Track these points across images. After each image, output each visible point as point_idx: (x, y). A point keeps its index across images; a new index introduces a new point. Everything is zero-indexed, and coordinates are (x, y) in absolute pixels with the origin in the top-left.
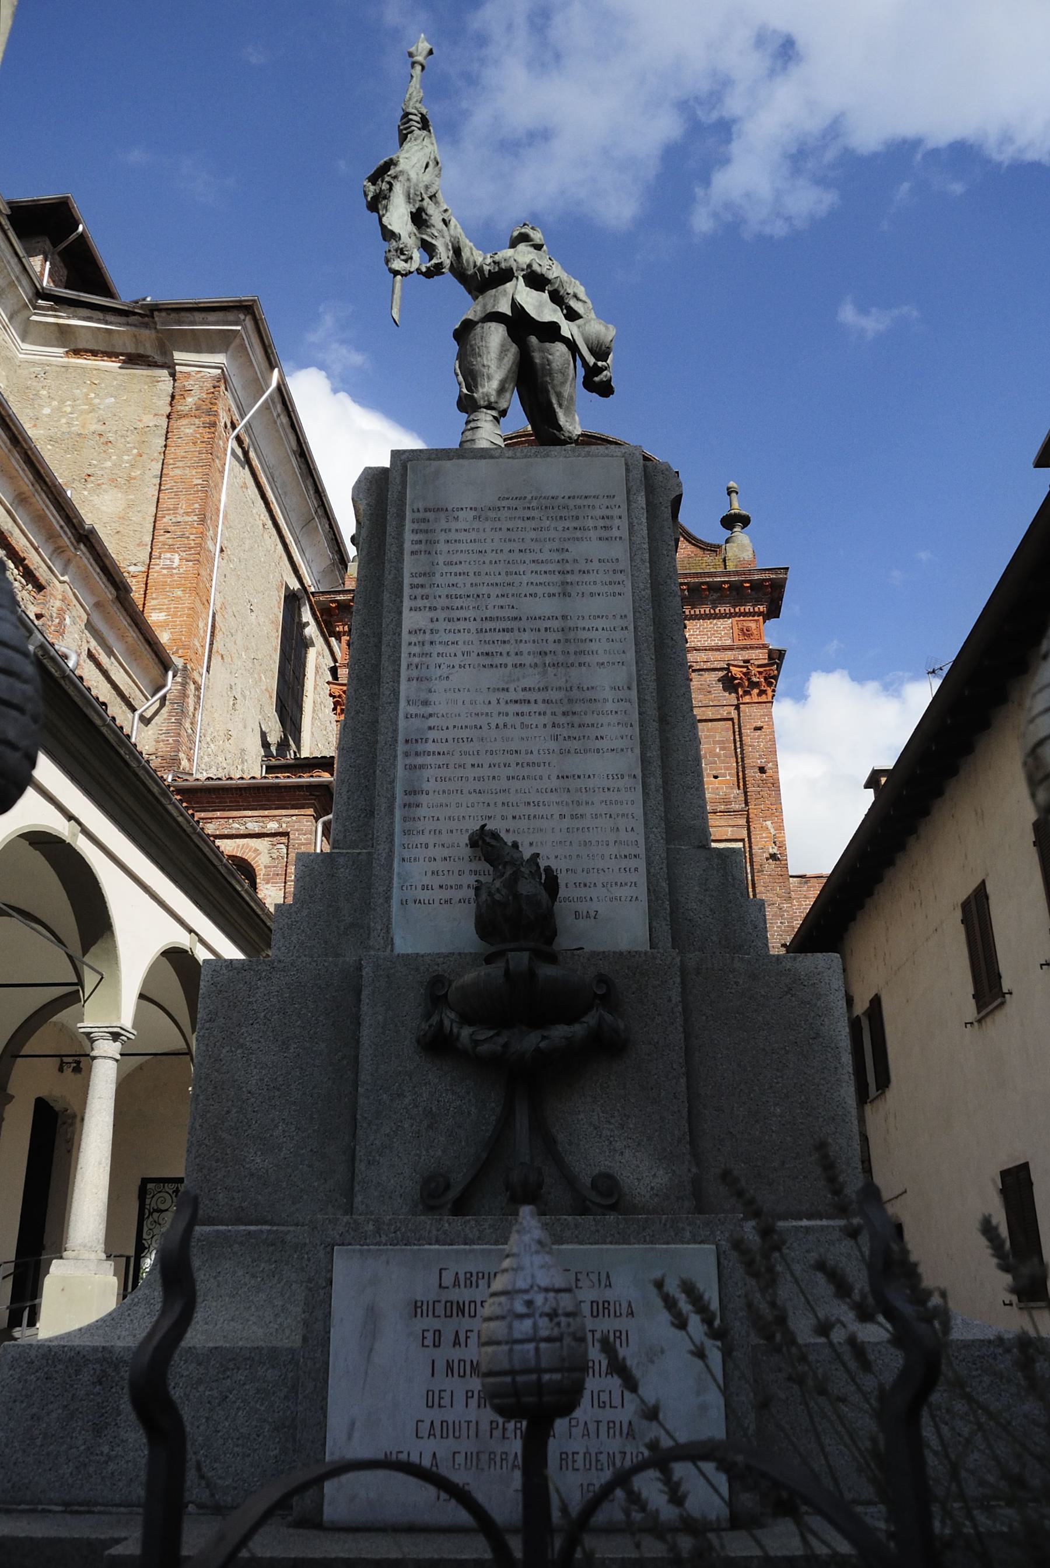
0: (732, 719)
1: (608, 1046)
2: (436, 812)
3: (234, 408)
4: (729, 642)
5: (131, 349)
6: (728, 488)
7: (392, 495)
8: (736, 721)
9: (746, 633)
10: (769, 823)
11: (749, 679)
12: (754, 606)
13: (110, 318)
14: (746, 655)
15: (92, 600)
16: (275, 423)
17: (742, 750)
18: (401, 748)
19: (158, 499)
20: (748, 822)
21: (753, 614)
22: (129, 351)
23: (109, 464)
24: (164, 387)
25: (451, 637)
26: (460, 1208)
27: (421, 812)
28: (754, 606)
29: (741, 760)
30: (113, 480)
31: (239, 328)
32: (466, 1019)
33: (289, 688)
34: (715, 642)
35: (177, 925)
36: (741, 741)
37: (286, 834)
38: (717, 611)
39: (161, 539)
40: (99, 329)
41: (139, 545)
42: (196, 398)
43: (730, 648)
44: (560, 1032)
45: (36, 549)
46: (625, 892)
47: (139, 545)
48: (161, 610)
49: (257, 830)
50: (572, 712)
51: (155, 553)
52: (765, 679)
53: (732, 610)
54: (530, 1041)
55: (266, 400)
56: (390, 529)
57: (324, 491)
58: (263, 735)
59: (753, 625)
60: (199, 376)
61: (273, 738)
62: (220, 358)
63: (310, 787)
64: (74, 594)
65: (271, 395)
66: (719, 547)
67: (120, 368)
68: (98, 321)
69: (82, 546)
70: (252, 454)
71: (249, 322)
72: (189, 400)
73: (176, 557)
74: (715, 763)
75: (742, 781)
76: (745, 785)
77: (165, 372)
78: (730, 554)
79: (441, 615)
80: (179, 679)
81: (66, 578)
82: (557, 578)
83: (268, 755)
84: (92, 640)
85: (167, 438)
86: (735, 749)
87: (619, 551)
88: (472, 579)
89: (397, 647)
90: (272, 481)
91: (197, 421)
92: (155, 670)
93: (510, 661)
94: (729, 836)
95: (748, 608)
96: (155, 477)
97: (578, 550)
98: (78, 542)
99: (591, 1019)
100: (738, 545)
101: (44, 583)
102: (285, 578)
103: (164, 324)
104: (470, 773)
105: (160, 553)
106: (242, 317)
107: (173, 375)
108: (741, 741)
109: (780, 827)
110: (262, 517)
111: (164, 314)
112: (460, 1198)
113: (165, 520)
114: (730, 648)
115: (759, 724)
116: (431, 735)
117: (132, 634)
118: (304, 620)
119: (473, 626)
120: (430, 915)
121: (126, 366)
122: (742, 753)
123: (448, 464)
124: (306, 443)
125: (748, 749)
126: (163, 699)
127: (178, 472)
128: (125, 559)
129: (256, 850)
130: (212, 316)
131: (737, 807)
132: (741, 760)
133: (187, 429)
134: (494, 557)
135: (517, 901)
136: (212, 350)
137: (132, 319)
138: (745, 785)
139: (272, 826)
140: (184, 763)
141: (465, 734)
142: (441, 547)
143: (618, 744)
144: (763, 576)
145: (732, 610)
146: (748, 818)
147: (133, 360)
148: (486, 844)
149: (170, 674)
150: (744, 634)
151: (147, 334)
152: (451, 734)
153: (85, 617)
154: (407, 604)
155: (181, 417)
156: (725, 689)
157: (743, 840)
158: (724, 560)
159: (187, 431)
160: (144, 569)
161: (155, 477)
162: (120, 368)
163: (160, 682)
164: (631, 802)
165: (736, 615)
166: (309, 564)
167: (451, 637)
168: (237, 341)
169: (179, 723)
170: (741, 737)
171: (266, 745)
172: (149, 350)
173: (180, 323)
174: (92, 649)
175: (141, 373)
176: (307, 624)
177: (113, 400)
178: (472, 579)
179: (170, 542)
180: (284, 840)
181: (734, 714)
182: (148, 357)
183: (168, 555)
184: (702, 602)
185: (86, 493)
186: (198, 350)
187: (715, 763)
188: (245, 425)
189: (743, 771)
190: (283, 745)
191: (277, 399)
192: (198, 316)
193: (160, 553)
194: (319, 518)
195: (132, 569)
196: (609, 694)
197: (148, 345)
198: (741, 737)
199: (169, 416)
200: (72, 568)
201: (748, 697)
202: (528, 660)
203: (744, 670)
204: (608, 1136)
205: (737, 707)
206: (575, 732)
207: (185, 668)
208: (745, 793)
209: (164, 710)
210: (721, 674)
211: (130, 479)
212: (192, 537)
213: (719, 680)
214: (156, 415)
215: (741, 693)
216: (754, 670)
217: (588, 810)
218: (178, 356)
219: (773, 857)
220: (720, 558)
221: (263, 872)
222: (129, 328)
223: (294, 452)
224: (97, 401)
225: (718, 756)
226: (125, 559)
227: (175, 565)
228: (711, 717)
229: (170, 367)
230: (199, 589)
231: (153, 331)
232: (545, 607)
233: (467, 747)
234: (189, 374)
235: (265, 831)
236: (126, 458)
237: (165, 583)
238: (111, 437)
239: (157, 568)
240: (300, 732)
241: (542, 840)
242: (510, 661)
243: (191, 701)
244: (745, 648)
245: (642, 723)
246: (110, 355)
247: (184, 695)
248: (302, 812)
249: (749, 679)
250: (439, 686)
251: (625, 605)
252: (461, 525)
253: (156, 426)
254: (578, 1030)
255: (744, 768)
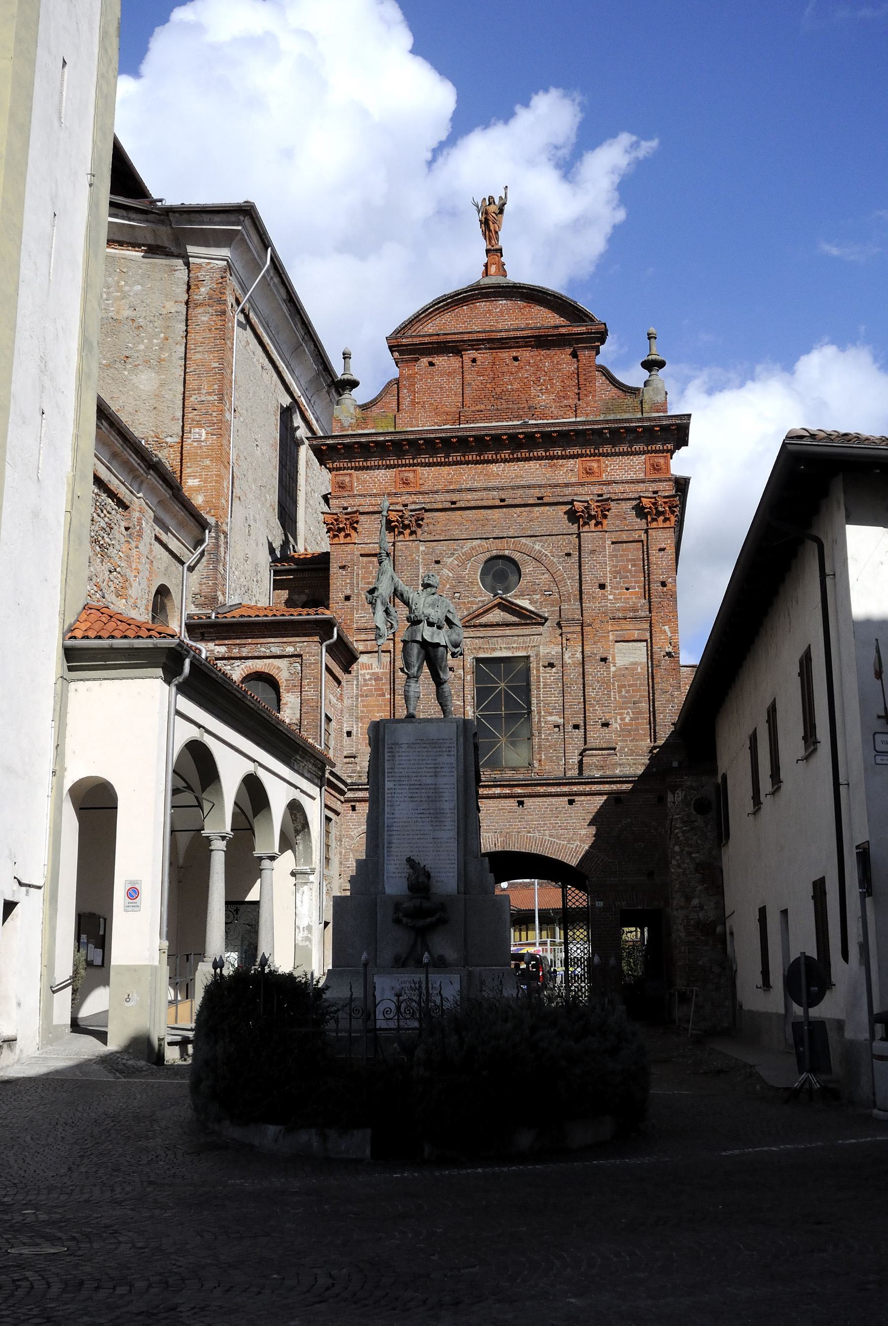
0: (642, 541)
1: (443, 922)
2: (397, 850)
3: (237, 287)
4: (642, 476)
5: (150, 241)
6: (648, 334)
7: (381, 729)
8: (645, 543)
9: (656, 468)
10: (666, 627)
11: (656, 508)
12: (663, 445)
13: (133, 215)
14: (654, 487)
15: (155, 501)
16: (269, 285)
17: (649, 568)
18: (386, 828)
19: (185, 378)
20: (651, 626)
21: (663, 451)
22: (150, 242)
23: (142, 347)
24: (180, 276)
25: (400, 791)
26: (404, 965)
27: (393, 849)
28: (663, 445)
29: (647, 575)
30: (146, 362)
31: (240, 228)
32: (405, 916)
33: (286, 490)
34: (631, 476)
35: (241, 749)
36: (648, 560)
37: (300, 656)
38: (633, 449)
39: (190, 415)
40: (124, 224)
41: (172, 419)
42: (208, 288)
43: (643, 481)
44: (429, 920)
45: (123, 483)
46: (452, 874)
47: (172, 419)
48: (195, 477)
49: (279, 653)
50: (436, 816)
51: (187, 428)
52: (670, 507)
53: (646, 449)
54: (421, 923)
55: (264, 276)
56: (381, 750)
57: (310, 322)
58: (270, 544)
59: (662, 461)
60: (209, 267)
61: (277, 544)
62: (225, 252)
63: (316, 622)
64: (147, 504)
65: (267, 270)
66: (638, 389)
67: (143, 257)
68: (123, 218)
69: (151, 472)
70: (252, 315)
71: (248, 222)
72: (203, 289)
73: (204, 431)
74: (627, 577)
75: (647, 593)
76: (649, 596)
77: (180, 262)
78: (646, 397)
79: (398, 783)
80: (213, 535)
81: (140, 495)
82: (433, 770)
83: (275, 560)
84: (157, 528)
85: (187, 326)
86: (644, 566)
87: (453, 760)
88: (407, 770)
89: (384, 793)
90: (267, 328)
91: (210, 310)
92: (196, 531)
93: (418, 799)
94: (636, 637)
95: (659, 446)
96: (180, 358)
97: (440, 759)
98: (148, 469)
99: (437, 916)
100: (653, 389)
101: (128, 503)
102: (280, 401)
103: (178, 223)
104: (406, 837)
105: (190, 428)
106: (242, 218)
107: (187, 264)
108: (648, 560)
109: (675, 631)
110: (261, 361)
111: (177, 215)
112: (400, 963)
113: (192, 399)
114: (643, 481)
115: (663, 546)
116: (395, 824)
117: (182, 514)
118: (296, 425)
119: (407, 787)
120: (395, 883)
121: (150, 255)
122: (648, 570)
123: (399, 725)
124: (295, 293)
125: (653, 567)
126: (202, 554)
127: (198, 356)
128: (162, 432)
129: (278, 668)
130: (217, 218)
131: (643, 614)
132: (647, 575)
133: (203, 317)
134: (413, 762)
135: (420, 880)
136: (218, 245)
137: (150, 217)
138: (649, 596)
139: (290, 650)
140: (221, 598)
141: (405, 824)
142: (397, 758)
143: (450, 828)
144: (670, 422)
145: (646, 449)
146: (651, 623)
147: (153, 250)
148: (410, 861)
149: (207, 531)
150: (655, 469)
151: (163, 230)
152: (402, 824)
153: (152, 514)
154: (386, 779)
155: (197, 305)
156: (637, 516)
157: (646, 641)
158: (641, 402)
159: (203, 318)
160: (178, 440)
161: (180, 358)
162: (143, 257)
163: (200, 537)
164: (453, 846)
165: (648, 452)
166: (297, 380)
167: (400, 791)
168: (238, 237)
169: (215, 569)
170: (648, 557)
171: (272, 551)
172: (167, 243)
173: (191, 223)
174: (158, 535)
175: (161, 262)
176: (298, 427)
177: (139, 287)
178: (407, 770)
179: (197, 418)
180: (298, 660)
181: (644, 537)
182: (166, 248)
183: (197, 430)
184: (621, 442)
185: (126, 373)
186: (207, 245)
187: (627, 577)
188: (248, 300)
189: (649, 585)
190: (285, 544)
191: (272, 272)
192: (206, 217)
193: (190, 428)
194: (306, 342)
195: (169, 440)
196: (448, 811)
197: (165, 238)
198: (648, 557)
199: (187, 303)
200: (144, 486)
201: (655, 523)
202: (424, 799)
203: (653, 500)
204: (443, 945)
205: (646, 531)
206: (438, 824)
207: (217, 525)
208: (650, 602)
209: (204, 559)
210: (635, 503)
211: (160, 360)
212: (214, 414)
213: (633, 508)
214: (176, 302)
215: (649, 520)
216: (660, 501)
217: (441, 849)
218: (191, 249)
219: (669, 654)
220: (638, 400)
221: (284, 684)
222: (149, 224)
223: (284, 301)
224: (127, 288)
225: (630, 571)
226: (162, 432)
227: (203, 438)
228: (625, 539)
229: (185, 258)
230: (221, 457)
231: (169, 228)
232: (429, 781)
233: (405, 828)
234: (200, 265)
235: (284, 653)
236: (155, 341)
237: (196, 454)
238: (141, 321)
239: (189, 441)
240: (296, 523)
241: (426, 861)
242: (418, 799)
243: (222, 549)
244: (654, 481)
245: (458, 820)
246: (134, 245)
247: (217, 546)
248: (311, 639)
249: (656, 508)
250: (397, 808)
251: (454, 780)
252: (404, 750)
253: (177, 312)
254: (434, 919)
255: (649, 582)
